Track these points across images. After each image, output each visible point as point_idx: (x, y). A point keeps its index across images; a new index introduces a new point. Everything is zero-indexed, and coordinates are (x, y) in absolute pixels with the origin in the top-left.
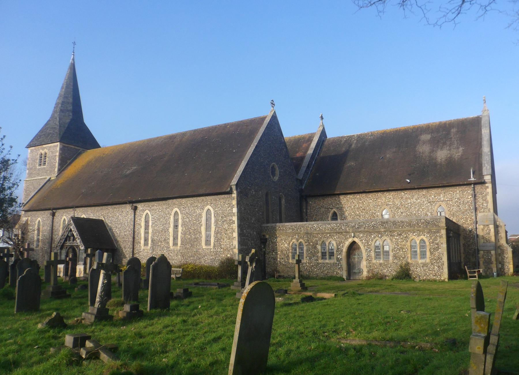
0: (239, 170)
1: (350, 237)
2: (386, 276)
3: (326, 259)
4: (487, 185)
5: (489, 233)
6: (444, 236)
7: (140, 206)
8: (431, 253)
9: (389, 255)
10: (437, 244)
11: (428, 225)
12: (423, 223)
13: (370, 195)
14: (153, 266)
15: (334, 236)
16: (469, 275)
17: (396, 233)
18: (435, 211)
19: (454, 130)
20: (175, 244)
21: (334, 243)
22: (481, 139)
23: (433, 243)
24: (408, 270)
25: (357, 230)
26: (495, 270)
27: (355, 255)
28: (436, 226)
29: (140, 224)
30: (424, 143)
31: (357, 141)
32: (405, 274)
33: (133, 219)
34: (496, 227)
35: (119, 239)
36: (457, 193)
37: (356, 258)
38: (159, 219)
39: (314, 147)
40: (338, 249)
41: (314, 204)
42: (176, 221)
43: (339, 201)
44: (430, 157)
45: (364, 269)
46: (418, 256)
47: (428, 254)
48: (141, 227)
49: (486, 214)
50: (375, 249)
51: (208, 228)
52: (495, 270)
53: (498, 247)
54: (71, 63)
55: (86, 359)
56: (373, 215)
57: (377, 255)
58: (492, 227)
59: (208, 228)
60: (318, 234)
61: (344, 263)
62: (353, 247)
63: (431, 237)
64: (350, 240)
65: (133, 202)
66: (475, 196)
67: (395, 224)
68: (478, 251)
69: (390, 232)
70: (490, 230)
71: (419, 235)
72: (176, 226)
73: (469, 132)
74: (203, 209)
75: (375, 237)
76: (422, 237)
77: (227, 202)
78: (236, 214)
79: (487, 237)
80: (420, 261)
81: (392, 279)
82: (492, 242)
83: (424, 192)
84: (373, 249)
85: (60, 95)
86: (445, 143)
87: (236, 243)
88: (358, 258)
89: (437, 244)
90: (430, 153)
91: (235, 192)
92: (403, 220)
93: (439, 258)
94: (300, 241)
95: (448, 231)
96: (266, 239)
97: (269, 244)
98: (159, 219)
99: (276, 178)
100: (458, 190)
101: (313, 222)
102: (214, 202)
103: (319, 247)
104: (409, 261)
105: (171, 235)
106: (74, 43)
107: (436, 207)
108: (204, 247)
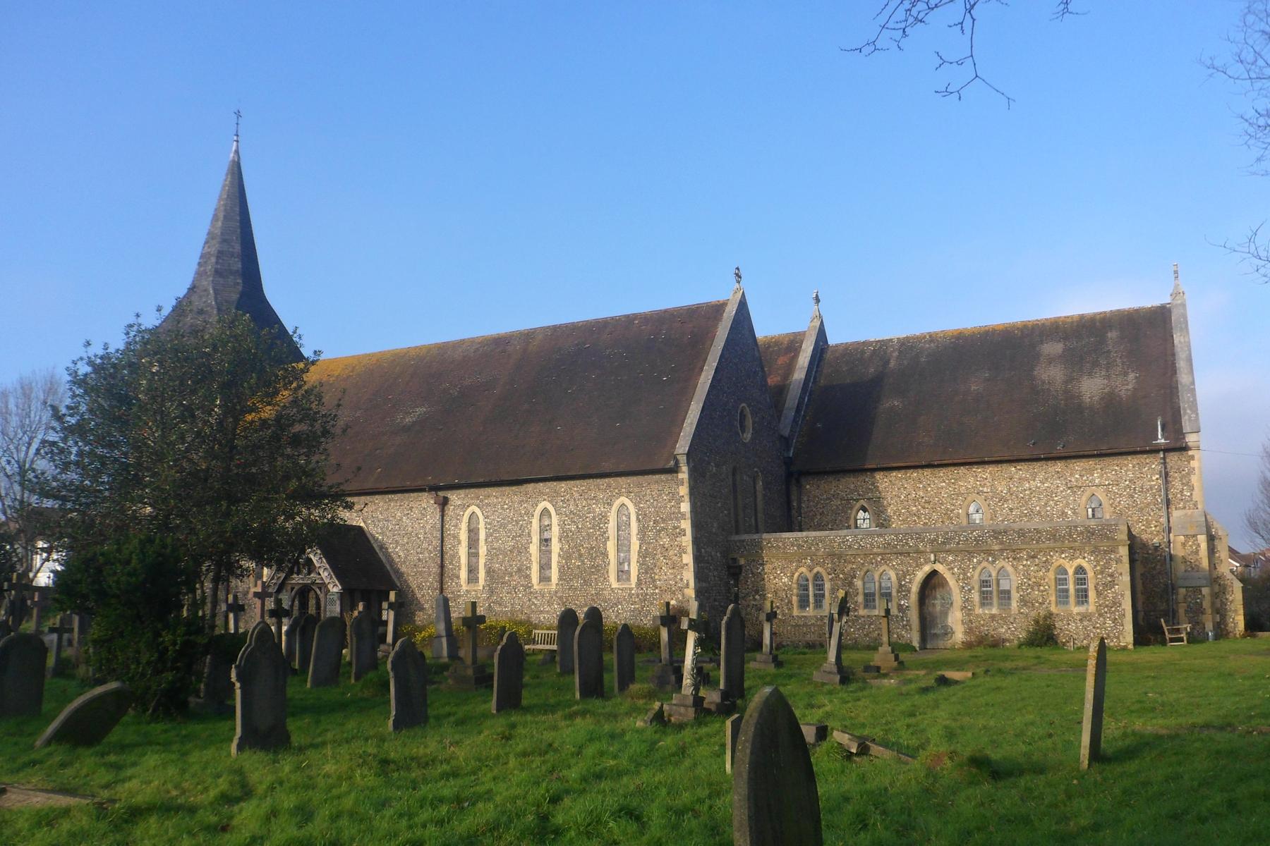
0: (688, 421)
1: (927, 561)
2: (1004, 641)
3: (874, 607)
4: (1190, 453)
5: (1197, 552)
6: (1126, 560)
7: (455, 497)
8: (1099, 594)
9: (1009, 598)
10: (1111, 575)
11: (1094, 538)
12: (1082, 533)
13: (942, 472)
14: (728, 624)
15: (891, 560)
16: (1168, 636)
17: (1024, 555)
18: (1082, 506)
19: (1112, 335)
20: (544, 579)
21: (892, 574)
22: (1173, 355)
23: (1102, 573)
24: (1050, 628)
25: (940, 548)
26: (1209, 626)
27: (935, 598)
28: (1108, 538)
29: (456, 537)
30: (1051, 360)
31: (900, 352)
32: (1044, 635)
33: (439, 526)
34: (1211, 539)
35: (403, 569)
36: (1128, 468)
37: (938, 605)
38: (503, 526)
39: (806, 364)
40: (901, 586)
41: (816, 491)
42: (544, 529)
43: (873, 484)
44: (1066, 392)
45: (956, 625)
46: (1072, 599)
47: (1092, 594)
48: (459, 542)
49: (1189, 512)
50: (981, 586)
51: (622, 545)
52: (1209, 626)
53: (1215, 581)
54: (233, 161)
55: (857, 754)
56: (947, 514)
57: (985, 599)
58: (1202, 539)
59: (622, 545)
60: (855, 556)
61: (914, 616)
62: (932, 582)
63: (1098, 562)
64: (927, 569)
65: (439, 489)
66: (1167, 474)
67: (1023, 535)
68: (1174, 588)
69: (1013, 552)
70: (1199, 545)
71: (1072, 558)
72: (546, 540)
73: (1147, 339)
74: (610, 505)
75: (979, 563)
76: (1079, 561)
77: (667, 491)
78: (688, 515)
79: (1192, 558)
80: (1076, 610)
81: (1020, 646)
82: (1203, 570)
83: (1059, 466)
84: (977, 587)
85: (211, 236)
86: (1095, 364)
87: (689, 576)
88: (942, 606)
89: (1111, 575)
90: (1066, 382)
91: (685, 468)
92: (1040, 527)
93: (1115, 603)
94: (815, 570)
95: (1131, 548)
96: (740, 567)
97: (746, 578)
98: (503, 526)
99: (748, 436)
100: (1130, 463)
101: (845, 532)
102: (636, 490)
103: (858, 583)
104: (1053, 609)
105: (533, 559)
106: (238, 114)
107: (1084, 498)
108: (615, 585)
